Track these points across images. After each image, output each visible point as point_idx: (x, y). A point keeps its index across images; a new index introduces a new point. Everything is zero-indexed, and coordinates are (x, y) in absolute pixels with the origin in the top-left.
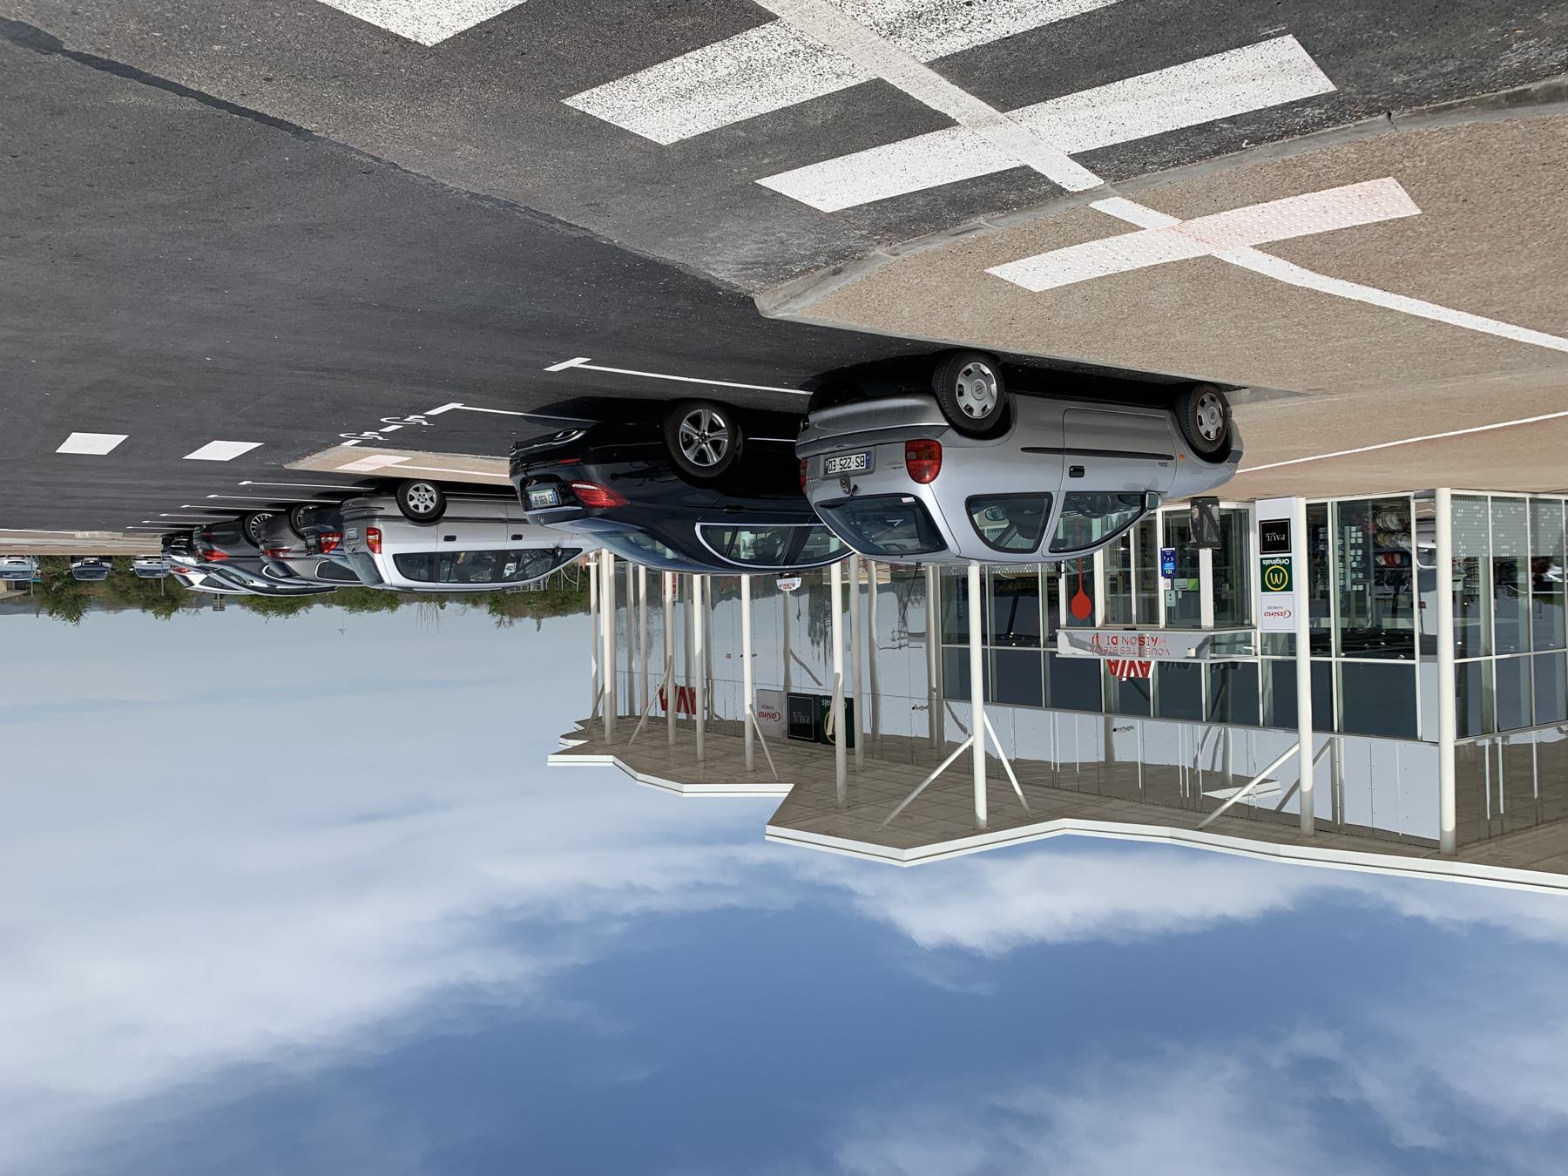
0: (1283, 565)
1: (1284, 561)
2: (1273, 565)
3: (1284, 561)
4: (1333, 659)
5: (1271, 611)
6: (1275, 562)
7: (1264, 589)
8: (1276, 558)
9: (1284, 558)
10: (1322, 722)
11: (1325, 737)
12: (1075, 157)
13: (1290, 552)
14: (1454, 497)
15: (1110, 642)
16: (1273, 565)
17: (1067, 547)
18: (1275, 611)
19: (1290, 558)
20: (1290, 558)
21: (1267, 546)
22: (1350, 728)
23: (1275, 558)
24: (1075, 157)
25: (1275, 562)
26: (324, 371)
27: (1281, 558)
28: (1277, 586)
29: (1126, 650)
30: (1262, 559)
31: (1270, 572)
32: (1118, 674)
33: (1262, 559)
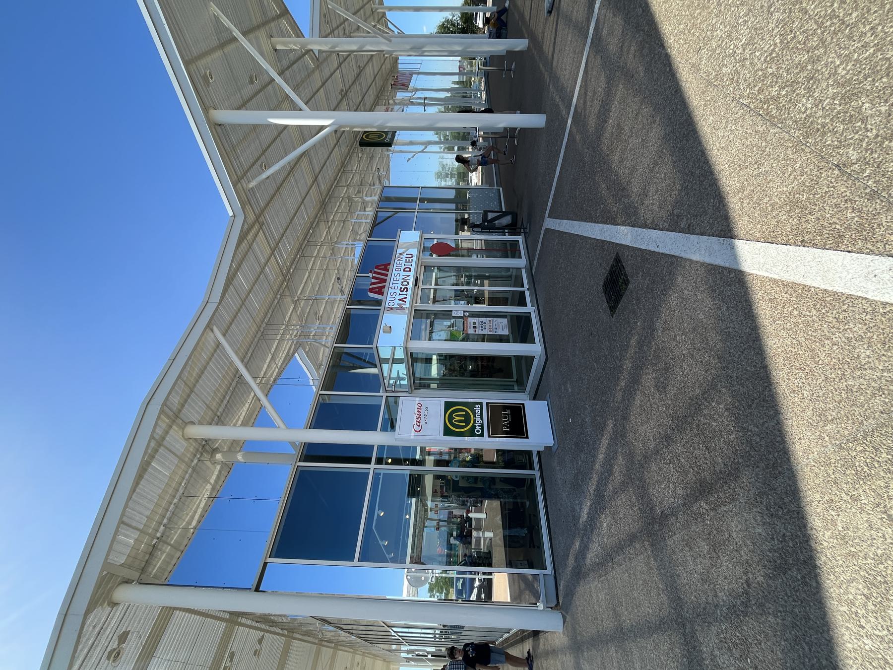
0: (474, 427)
1: (478, 428)
2: (474, 416)
3: (478, 428)
4: (372, 466)
5: (422, 411)
6: (478, 418)
7: (448, 405)
8: (481, 419)
9: (482, 429)
10: (312, 452)
11: (295, 453)
12: (613, 308)
13: (489, 436)
14: (366, 196)
15: (406, 266)
16: (474, 416)
17: (475, 269)
18: (423, 414)
19: (482, 435)
20: (482, 435)
21: (494, 410)
22: (302, 480)
23: (482, 418)
24: (613, 308)
25: (478, 418)
26: (469, 250)
27: (482, 426)
28: (451, 418)
29: (398, 277)
30: (481, 404)
31: (464, 410)
32: (376, 270)
33: (481, 404)
